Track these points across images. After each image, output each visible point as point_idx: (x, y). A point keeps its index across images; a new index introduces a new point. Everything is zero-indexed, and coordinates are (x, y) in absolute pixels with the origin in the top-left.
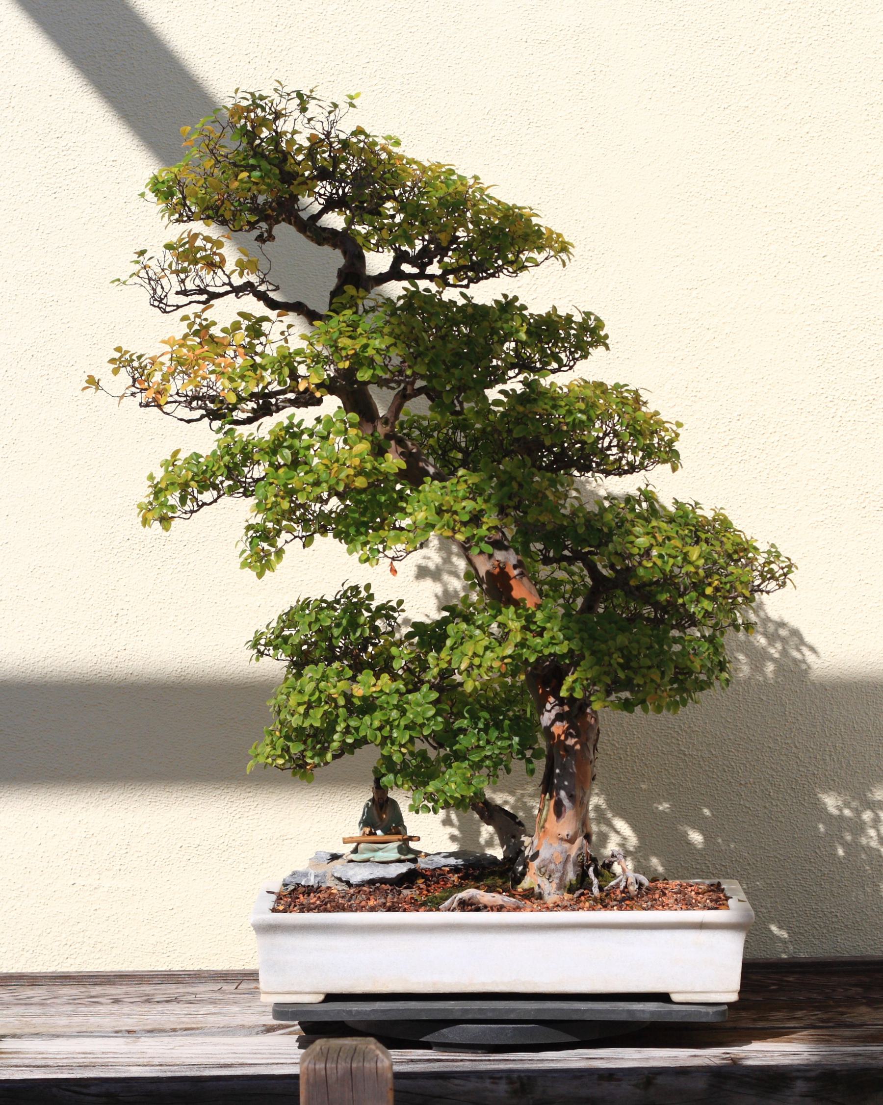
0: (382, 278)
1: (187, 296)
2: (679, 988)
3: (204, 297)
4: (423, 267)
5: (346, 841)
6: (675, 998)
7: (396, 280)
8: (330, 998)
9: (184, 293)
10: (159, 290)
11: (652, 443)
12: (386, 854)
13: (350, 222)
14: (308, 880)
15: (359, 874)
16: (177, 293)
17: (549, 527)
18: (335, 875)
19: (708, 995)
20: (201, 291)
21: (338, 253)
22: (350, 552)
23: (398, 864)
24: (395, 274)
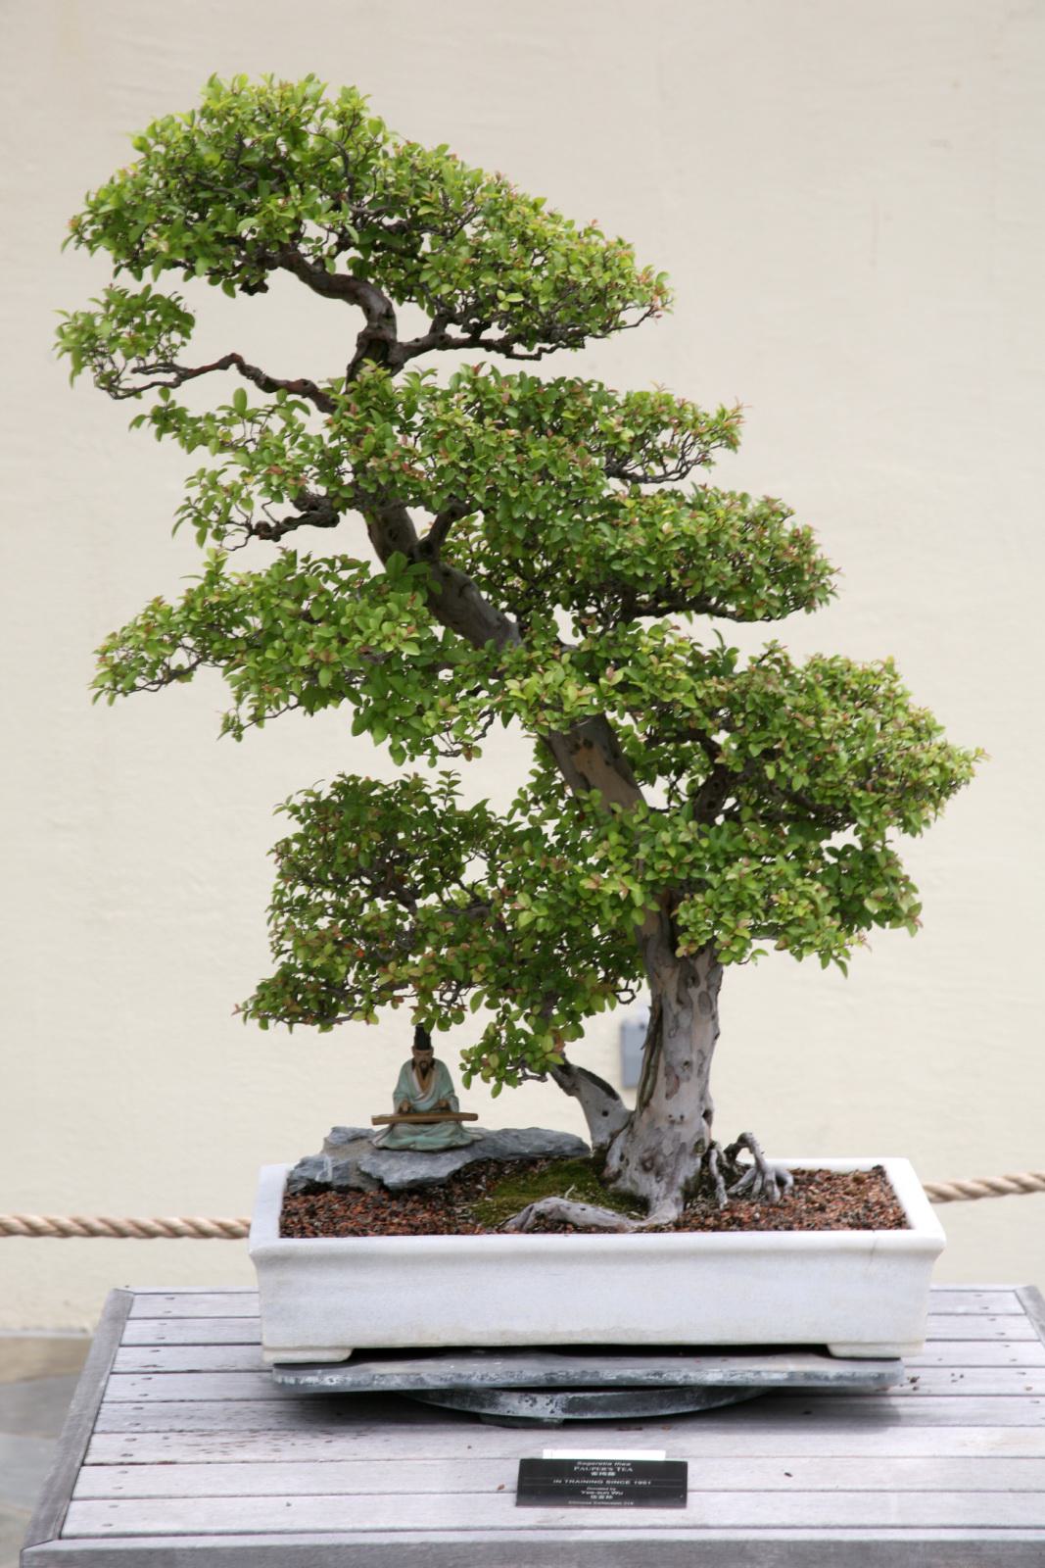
0: (419, 348)
1: (148, 373)
2: (841, 1338)
3: (171, 377)
4: (476, 330)
5: (377, 1121)
6: (835, 1350)
7: (439, 348)
8: (362, 1355)
9: (145, 370)
10: (108, 368)
11: (789, 578)
12: (431, 1139)
13: (563, 1482)
14: (324, 1174)
15: (399, 1172)
16: (134, 371)
17: (609, 670)
18: (363, 1169)
19: (881, 1347)
20: (169, 367)
21: (357, 311)
22: (368, 778)
23: (449, 1155)
24: (437, 340)
